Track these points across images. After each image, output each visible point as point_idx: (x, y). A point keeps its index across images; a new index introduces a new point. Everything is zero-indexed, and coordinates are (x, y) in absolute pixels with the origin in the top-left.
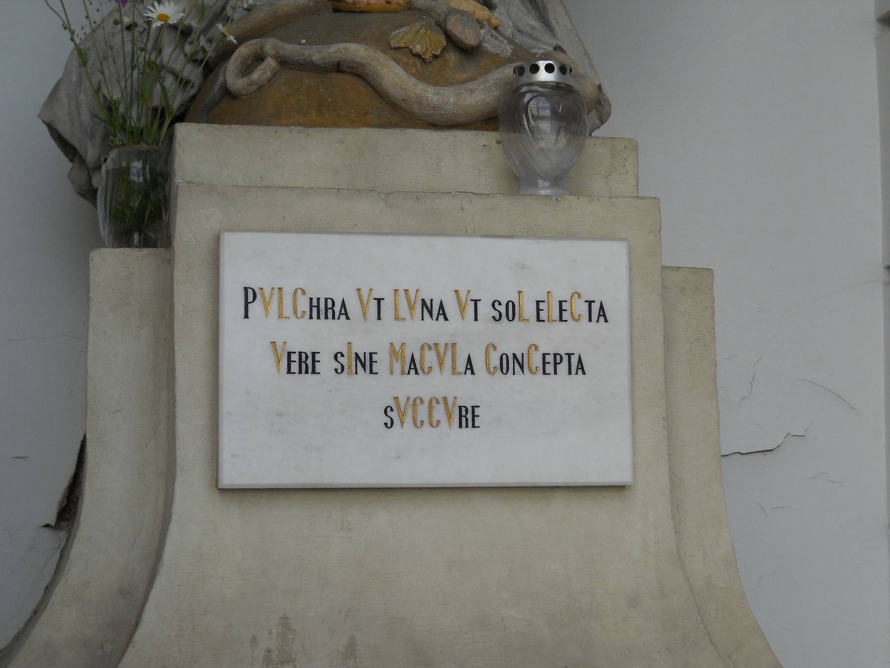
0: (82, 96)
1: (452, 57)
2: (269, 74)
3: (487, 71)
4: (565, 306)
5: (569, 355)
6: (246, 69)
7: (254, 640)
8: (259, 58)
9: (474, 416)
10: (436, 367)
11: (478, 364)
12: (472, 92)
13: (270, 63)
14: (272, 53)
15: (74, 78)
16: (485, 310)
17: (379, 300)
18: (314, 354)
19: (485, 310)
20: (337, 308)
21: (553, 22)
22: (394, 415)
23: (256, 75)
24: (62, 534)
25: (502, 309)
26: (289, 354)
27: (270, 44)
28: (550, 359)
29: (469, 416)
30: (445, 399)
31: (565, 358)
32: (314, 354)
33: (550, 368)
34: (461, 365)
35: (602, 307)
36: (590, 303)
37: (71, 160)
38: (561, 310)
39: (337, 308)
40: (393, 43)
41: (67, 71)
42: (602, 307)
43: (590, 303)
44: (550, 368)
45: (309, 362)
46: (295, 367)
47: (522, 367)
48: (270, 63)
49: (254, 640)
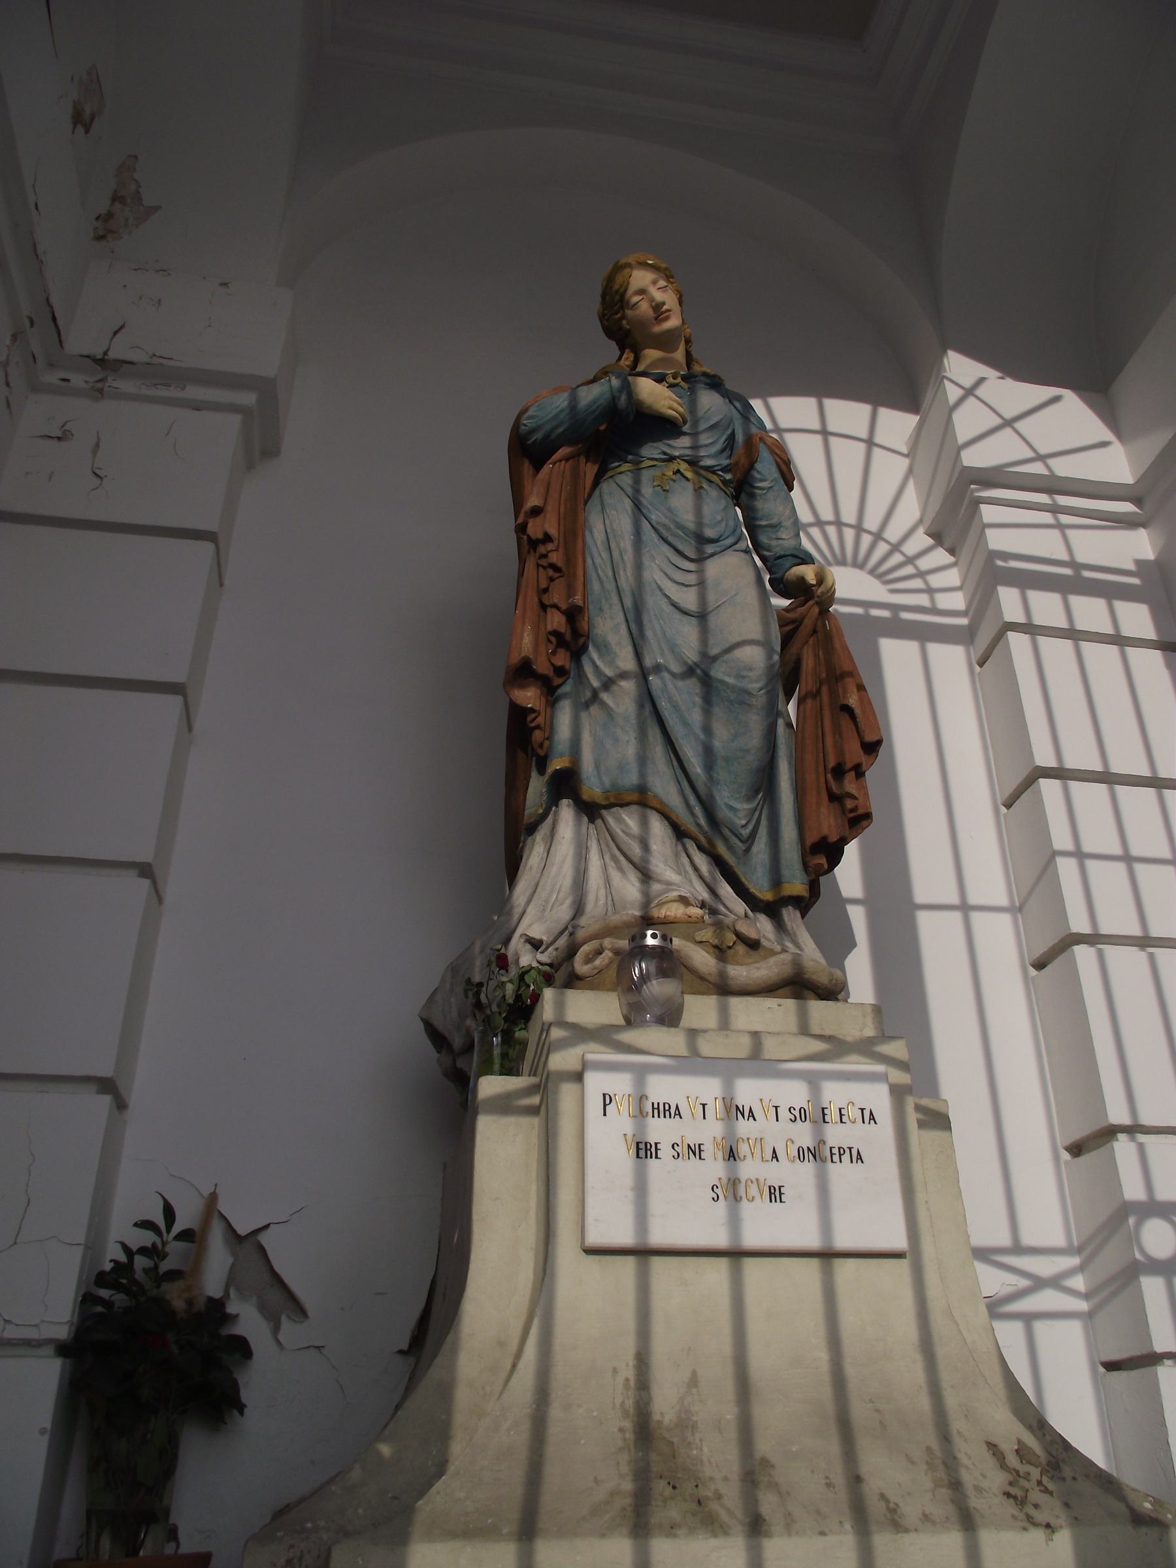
0: (453, 1000)
1: (741, 949)
2: (607, 961)
3: (765, 958)
4: (843, 1112)
5: (850, 1149)
6: (588, 960)
7: (615, 1371)
8: (599, 952)
9: (780, 1194)
10: (749, 1155)
11: (781, 1154)
12: (758, 968)
13: (607, 954)
14: (609, 947)
15: (448, 986)
16: (784, 1113)
17: (704, 1105)
18: (656, 1144)
19: (784, 1113)
20: (673, 1111)
21: (802, 944)
22: (719, 1191)
23: (597, 962)
24: (412, 1360)
25: (797, 1113)
26: (638, 1143)
27: (607, 942)
28: (835, 1151)
29: (777, 1193)
30: (757, 1180)
31: (847, 1151)
32: (656, 1144)
33: (836, 1158)
34: (768, 1154)
35: (871, 1113)
36: (862, 1110)
37: (439, 1052)
38: (841, 1115)
39: (673, 1111)
40: (698, 939)
41: (443, 981)
42: (871, 1113)
43: (862, 1110)
44: (836, 1158)
45: (653, 1150)
46: (642, 1153)
47: (815, 1157)
48: (607, 954)
49: (615, 1371)
